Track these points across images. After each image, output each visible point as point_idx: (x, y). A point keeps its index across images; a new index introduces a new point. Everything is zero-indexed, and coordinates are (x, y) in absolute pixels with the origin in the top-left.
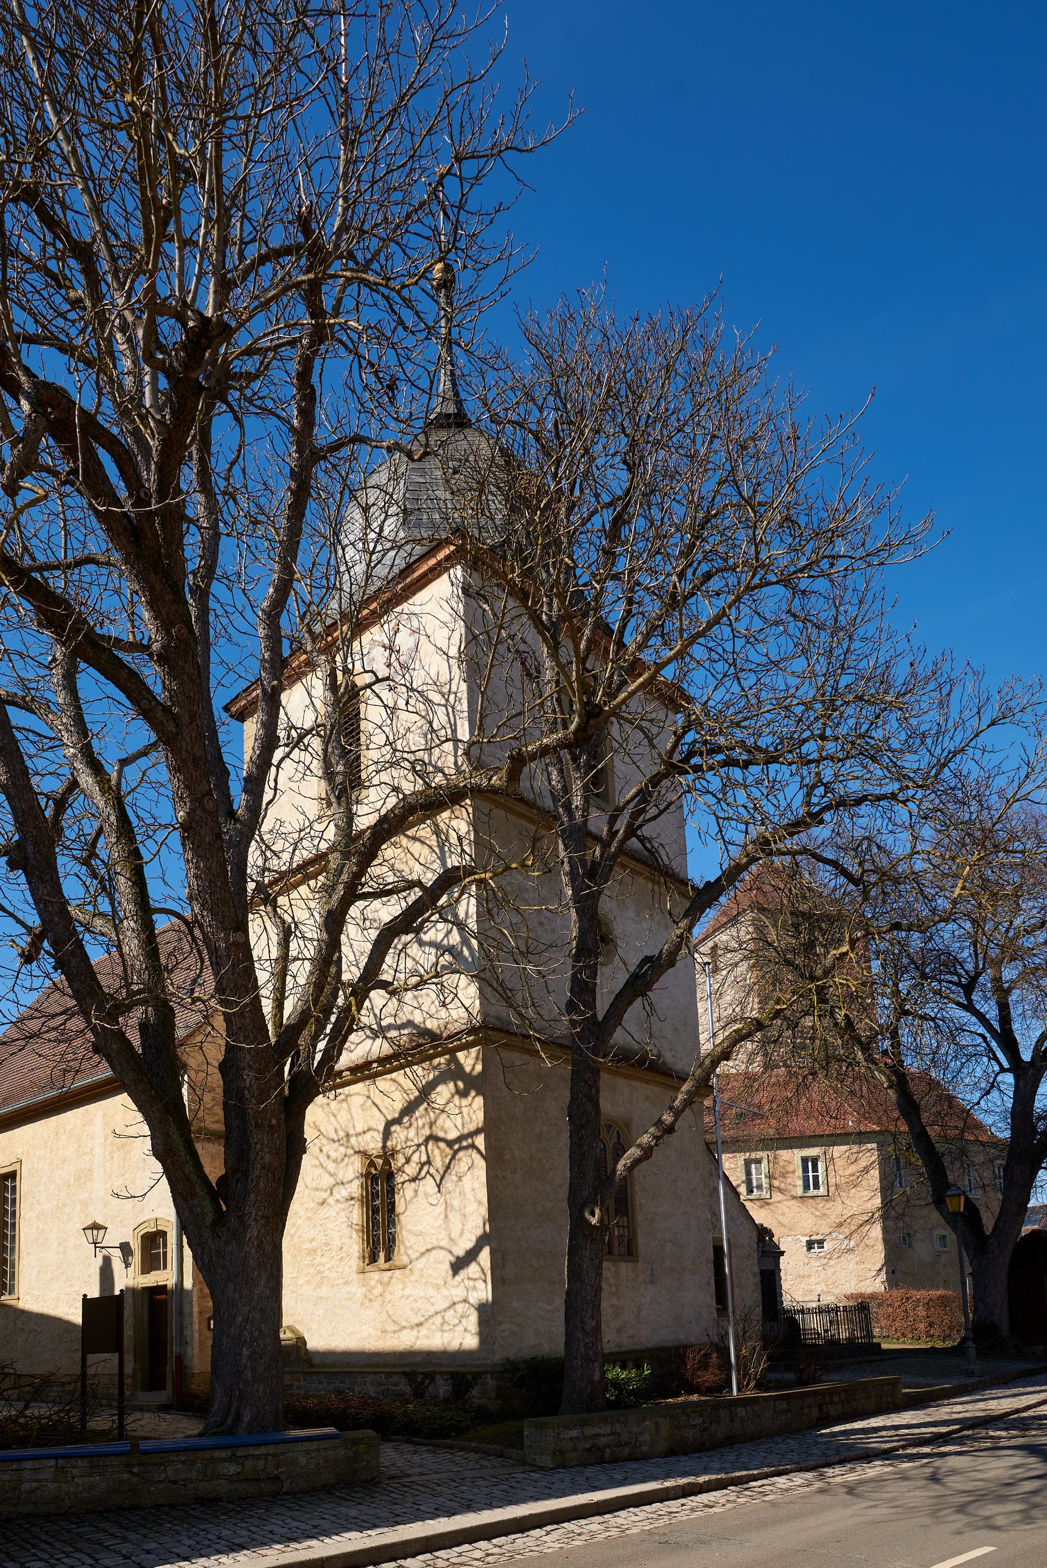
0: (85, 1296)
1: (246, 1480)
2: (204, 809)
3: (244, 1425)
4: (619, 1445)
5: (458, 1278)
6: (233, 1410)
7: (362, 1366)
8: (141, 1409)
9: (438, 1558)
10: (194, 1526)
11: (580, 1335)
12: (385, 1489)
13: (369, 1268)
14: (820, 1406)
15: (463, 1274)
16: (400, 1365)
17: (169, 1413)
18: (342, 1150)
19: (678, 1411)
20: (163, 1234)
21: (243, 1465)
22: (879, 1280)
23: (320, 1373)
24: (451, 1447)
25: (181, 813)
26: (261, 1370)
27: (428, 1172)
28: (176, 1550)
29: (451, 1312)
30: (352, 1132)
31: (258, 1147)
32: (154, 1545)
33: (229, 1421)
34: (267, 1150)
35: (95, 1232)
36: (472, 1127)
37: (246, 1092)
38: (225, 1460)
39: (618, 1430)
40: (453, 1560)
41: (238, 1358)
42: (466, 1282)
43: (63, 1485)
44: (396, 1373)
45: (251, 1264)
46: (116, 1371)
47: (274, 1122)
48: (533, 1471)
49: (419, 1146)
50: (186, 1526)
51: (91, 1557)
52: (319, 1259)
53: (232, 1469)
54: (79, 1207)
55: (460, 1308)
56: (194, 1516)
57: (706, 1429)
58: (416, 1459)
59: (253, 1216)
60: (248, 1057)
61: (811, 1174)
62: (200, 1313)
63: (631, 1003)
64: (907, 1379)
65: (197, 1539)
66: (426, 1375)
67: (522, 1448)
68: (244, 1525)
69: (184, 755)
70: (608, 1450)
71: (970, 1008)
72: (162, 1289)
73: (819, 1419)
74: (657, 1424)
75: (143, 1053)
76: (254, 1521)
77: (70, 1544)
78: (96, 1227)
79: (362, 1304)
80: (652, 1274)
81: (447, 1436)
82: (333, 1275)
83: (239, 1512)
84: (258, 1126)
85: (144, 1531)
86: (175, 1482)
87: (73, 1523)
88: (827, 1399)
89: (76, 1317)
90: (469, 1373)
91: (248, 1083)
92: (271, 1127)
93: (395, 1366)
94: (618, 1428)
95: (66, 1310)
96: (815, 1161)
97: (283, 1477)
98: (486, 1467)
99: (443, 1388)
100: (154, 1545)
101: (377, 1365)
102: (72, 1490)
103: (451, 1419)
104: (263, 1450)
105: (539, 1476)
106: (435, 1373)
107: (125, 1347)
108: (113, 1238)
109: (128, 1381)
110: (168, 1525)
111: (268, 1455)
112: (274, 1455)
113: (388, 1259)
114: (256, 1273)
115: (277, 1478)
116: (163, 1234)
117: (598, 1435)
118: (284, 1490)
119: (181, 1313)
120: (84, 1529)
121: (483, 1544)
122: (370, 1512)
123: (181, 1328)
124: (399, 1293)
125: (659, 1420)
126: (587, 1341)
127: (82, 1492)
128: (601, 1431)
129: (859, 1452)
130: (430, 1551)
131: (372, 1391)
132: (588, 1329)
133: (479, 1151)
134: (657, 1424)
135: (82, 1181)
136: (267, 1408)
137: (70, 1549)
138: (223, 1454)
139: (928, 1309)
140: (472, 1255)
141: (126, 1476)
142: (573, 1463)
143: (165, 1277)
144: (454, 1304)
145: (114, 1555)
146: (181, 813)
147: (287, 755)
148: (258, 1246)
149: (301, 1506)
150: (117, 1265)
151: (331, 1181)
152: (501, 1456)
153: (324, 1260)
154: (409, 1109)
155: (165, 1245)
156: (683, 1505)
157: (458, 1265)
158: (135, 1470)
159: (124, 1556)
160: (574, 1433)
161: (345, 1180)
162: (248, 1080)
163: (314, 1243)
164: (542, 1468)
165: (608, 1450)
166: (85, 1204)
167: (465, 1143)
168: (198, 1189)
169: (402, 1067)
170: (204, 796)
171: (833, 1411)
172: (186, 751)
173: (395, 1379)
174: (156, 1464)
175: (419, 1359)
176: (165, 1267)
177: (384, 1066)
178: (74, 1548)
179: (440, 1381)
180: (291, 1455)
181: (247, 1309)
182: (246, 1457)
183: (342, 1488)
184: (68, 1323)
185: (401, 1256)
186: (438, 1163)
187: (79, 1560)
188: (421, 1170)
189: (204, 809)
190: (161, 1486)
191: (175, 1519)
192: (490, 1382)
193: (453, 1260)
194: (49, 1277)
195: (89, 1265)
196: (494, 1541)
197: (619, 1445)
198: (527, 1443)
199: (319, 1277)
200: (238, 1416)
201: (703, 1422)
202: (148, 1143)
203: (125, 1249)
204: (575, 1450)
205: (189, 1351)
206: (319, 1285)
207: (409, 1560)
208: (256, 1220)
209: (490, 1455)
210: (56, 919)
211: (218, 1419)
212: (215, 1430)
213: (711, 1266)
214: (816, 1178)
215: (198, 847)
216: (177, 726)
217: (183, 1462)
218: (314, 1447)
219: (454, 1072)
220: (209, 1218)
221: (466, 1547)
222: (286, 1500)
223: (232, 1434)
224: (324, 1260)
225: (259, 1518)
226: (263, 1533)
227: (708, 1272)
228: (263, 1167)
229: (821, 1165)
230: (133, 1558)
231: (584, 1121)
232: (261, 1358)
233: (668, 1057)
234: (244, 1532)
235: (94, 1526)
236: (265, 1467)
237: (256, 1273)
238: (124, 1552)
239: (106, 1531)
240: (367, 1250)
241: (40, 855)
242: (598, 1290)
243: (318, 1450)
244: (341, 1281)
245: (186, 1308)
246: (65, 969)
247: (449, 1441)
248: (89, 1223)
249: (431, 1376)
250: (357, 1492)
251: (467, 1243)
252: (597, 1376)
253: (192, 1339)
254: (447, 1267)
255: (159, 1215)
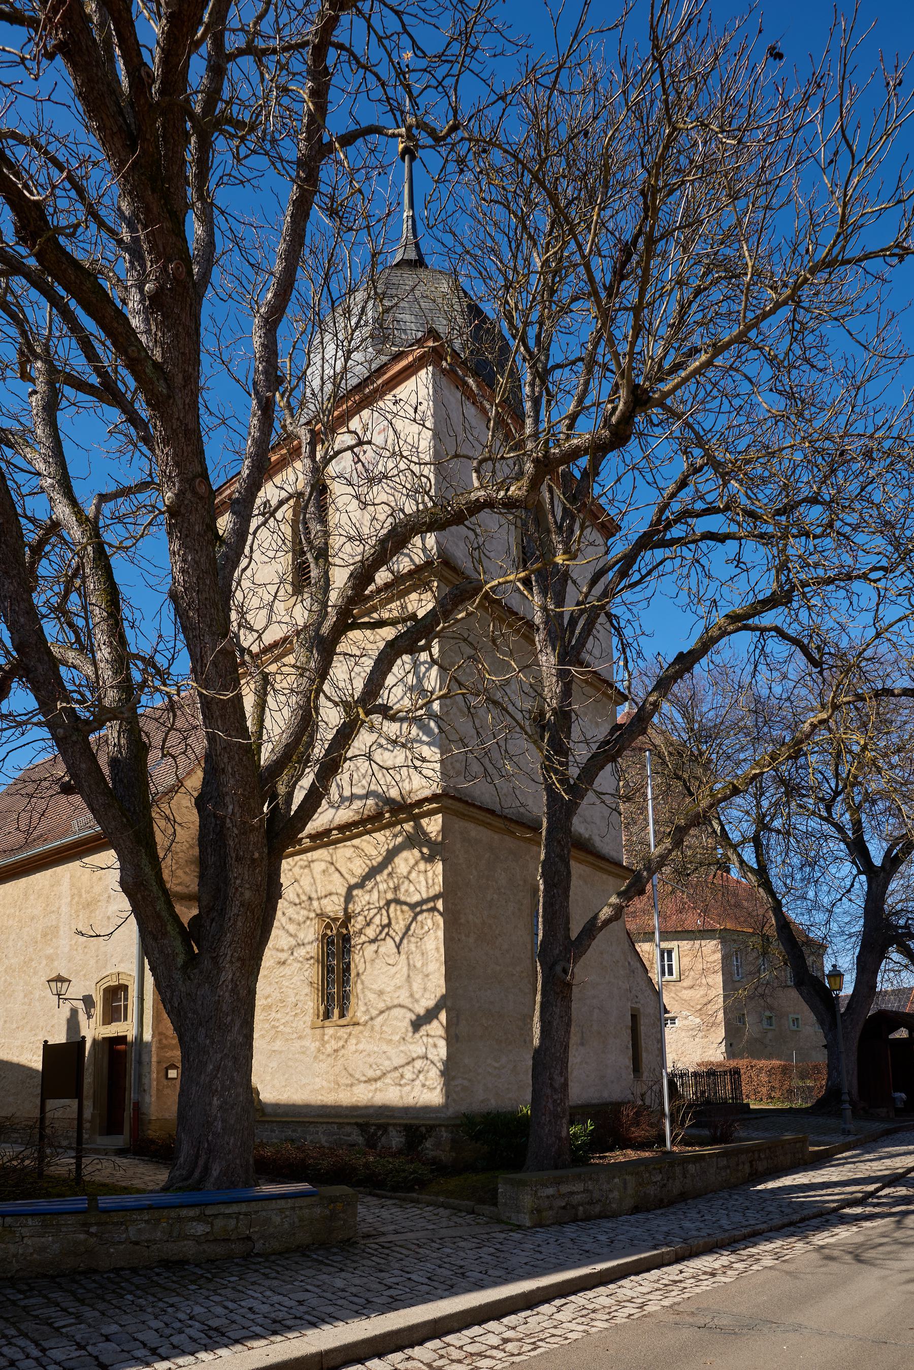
0: (46, 1042)
1: (215, 1240)
2: (194, 492)
3: (212, 1180)
4: (591, 1203)
5: (417, 1036)
6: (201, 1162)
7: (314, 1116)
8: (96, 1151)
9: (449, 1345)
10: (160, 1300)
11: (549, 1091)
12: (364, 1251)
13: (327, 1023)
14: (751, 1162)
15: (423, 1030)
16: (353, 1117)
17: (126, 1157)
18: (304, 913)
19: (642, 1168)
20: (125, 988)
21: (212, 1225)
22: (719, 1052)
23: (272, 1122)
24: (417, 1201)
25: (169, 494)
26: (232, 1122)
27: (387, 934)
28: (139, 1336)
29: (410, 1067)
30: (314, 895)
31: (238, 882)
32: (114, 1328)
33: (196, 1175)
34: (247, 886)
35: (59, 984)
36: (432, 893)
37: (228, 821)
38: (192, 1219)
39: (590, 1188)
40: (469, 1348)
41: (208, 1108)
42: (425, 1039)
43: (11, 1246)
44: (348, 1124)
45: (224, 1008)
46: (75, 1116)
47: (256, 855)
48: (511, 1230)
49: (380, 908)
50: (151, 1299)
51: (37, 1345)
52: (273, 1014)
53: (200, 1229)
54: (44, 962)
55: (418, 1064)
56: (159, 1285)
57: (664, 1185)
58: (385, 1214)
59: (228, 958)
60: (232, 782)
61: (666, 963)
62: (159, 1062)
63: (602, 768)
64: (812, 1137)
65: (166, 1318)
66: (379, 1126)
67: (495, 1204)
68: (217, 1298)
69: (176, 424)
70: (581, 1208)
71: (828, 820)
72: (122, 1039)
73: (750, 1175)
74: (625, 1183)
75: (114, 788)
76: (228, 1292)
77: (13, 1324)
78: (60, 979)
79: (316, 1057)
80: (582, 1037)
81: (411, 1190)
82: (288, 1030)
83: (210, 1280)
84: (238, 859)
85: (102, 1306)
86: (137, 1243)
87: (20, 1292)
88: (756, 1155)
89: (36, 1062)
90: (423, 1125)
91: (230, 810)
92: (253, 860)
93: (347, 1116)
94: (590, 1185)
95: (30, 1057)
96: (670, 952)
97: (255, 1237)
98: (461, 1225)
99: (396, 1140)
100: (114, 1328)
101: (328, 1116)
102: (21, 1251)
103: (414, 1172)
104: (235, 1208)
105: (520, 1236)
106: (388, 1124)
107: (85, 1093)
108: (76, 990)
109: (87, 1125)
110: (129, 1297)
111: (240, 1213)
112: (246, 1214)
113: (342, 1015)
114: (229, 1018)
115: (249, 1238)
116: (125, 988)
117: (572, 1193)
118: (255, 1251)
119: (140, 1062)
120: (32, 1301)
121: (492, 1325)
122: (357, 1281)
123: (140, 1077)
124: (353, 1048)
125: (627, 1177)
126: (555, 1097)
127: (32, 1254)
128: (575, 1189)
129: (815, 1210)
130: (439, 1336)
131: (323, 1140)
132: (557, 1086)
133: (438, 911)
134: (625, 1183)
135: (49, 937)
136: (238, 1161)
137: (13, 1332)
138: (192, 1213)
139: (770, 1076)
140: (430, 1015)
141: (82, 1236)
142: (548, 1222)
143: (126, 1028)
144: (413, 1060)
145: (65, 1342)
146: (169, 494)
147: (264, 523)
148: (232, 990)
149: (278, 1272)
150: (82, 1016)
151: (293, 942)
152: (473, 1212)
153: (279, 1016)
154: (373, 873)
155: (126, 999)
156: (681, 1272)
157: (417, 1024)
158: (93, 1229)
159: (78, 1344)
160: (550, 1191)
161: (306, 941)
162: (231, 807)
163: (269, 1000)
164: (519, 1227)
165: (581, 1208)
166: (51, 959)
167: (424, 907)
168: (169, 928)
169: (369, 832)
170: (195, 477)
171: (761, 1166)
172: (178, 419)
173: (348, 1129)
174: (113, 1223)
175: (371, 1111)
176: (126, 1019)
177: (344, 833)
178: (19, 1330)
179: (393, 1132)
180: (264, 1213)
181: (219, 1056)
182: (216, 1216)
183: (317, 1249)
184: (30, 1069)
185: (359, 1009)
186: (399, 926)
187: (22, 1349)
188: (381, 932)
189: (194, 492)
190: (122, 1247)
191: (138, 1288)
192: (445, 1135)
193: (414, 1017)
194: (14, 1026)
195: (53, 1016)
196: (505, 1320)
197: (591, 1203)
198: (501, 1200)
199: (273, 1032)
200: (207, 1169)
201: (662, 1179)
202: (117, 875)
203: (88, 1001)
204: (551, 1208)
205: (147, 1099)
206: (273, 1039)
207: (417, 1348)
208: (231, 962)
209: (460, 1211)
210: (22, 620)
211: (184, 1172)
212: (180, 1184)
213: (629, 1031)
214: (670, 967)
215: (187, 536)
216: (169, 387)
217: (147, 1222)
218: (289, 1205)
219: (416, 840)
220: (180, 960)
221: (476, 1330)
222: (259, 1263)
223: (200, 1189)
224: (279, 1016)
225: (233, 1288)
226: (242, 1311)
227: (626, 1037)
228: (242, 905)
229: (674, 955)
230: (89, 1348)
231: (556, 880)
232: (232, 1108)
233: (598, 842)
234: (219, 1310)
235: (45, 1297)
236: (237, 1228)
237: (229, 1018)
238: (78, 1337)
239: (58, 1305)
240: (322, 1008)
241: (7, 546)
242: (567, 1047)
243: (293, 1208)
244: (295, 1035)
245: (145, 1058)
246: (31, 676)
247: (415, 1195)
248: (54, 975)
249: (384, 1128)
250: (335, 1254)
251: (427, 1002)
252: (564, 1134)
253: (150, 1087)
254: (406, 1023)
255: (120, 970)
